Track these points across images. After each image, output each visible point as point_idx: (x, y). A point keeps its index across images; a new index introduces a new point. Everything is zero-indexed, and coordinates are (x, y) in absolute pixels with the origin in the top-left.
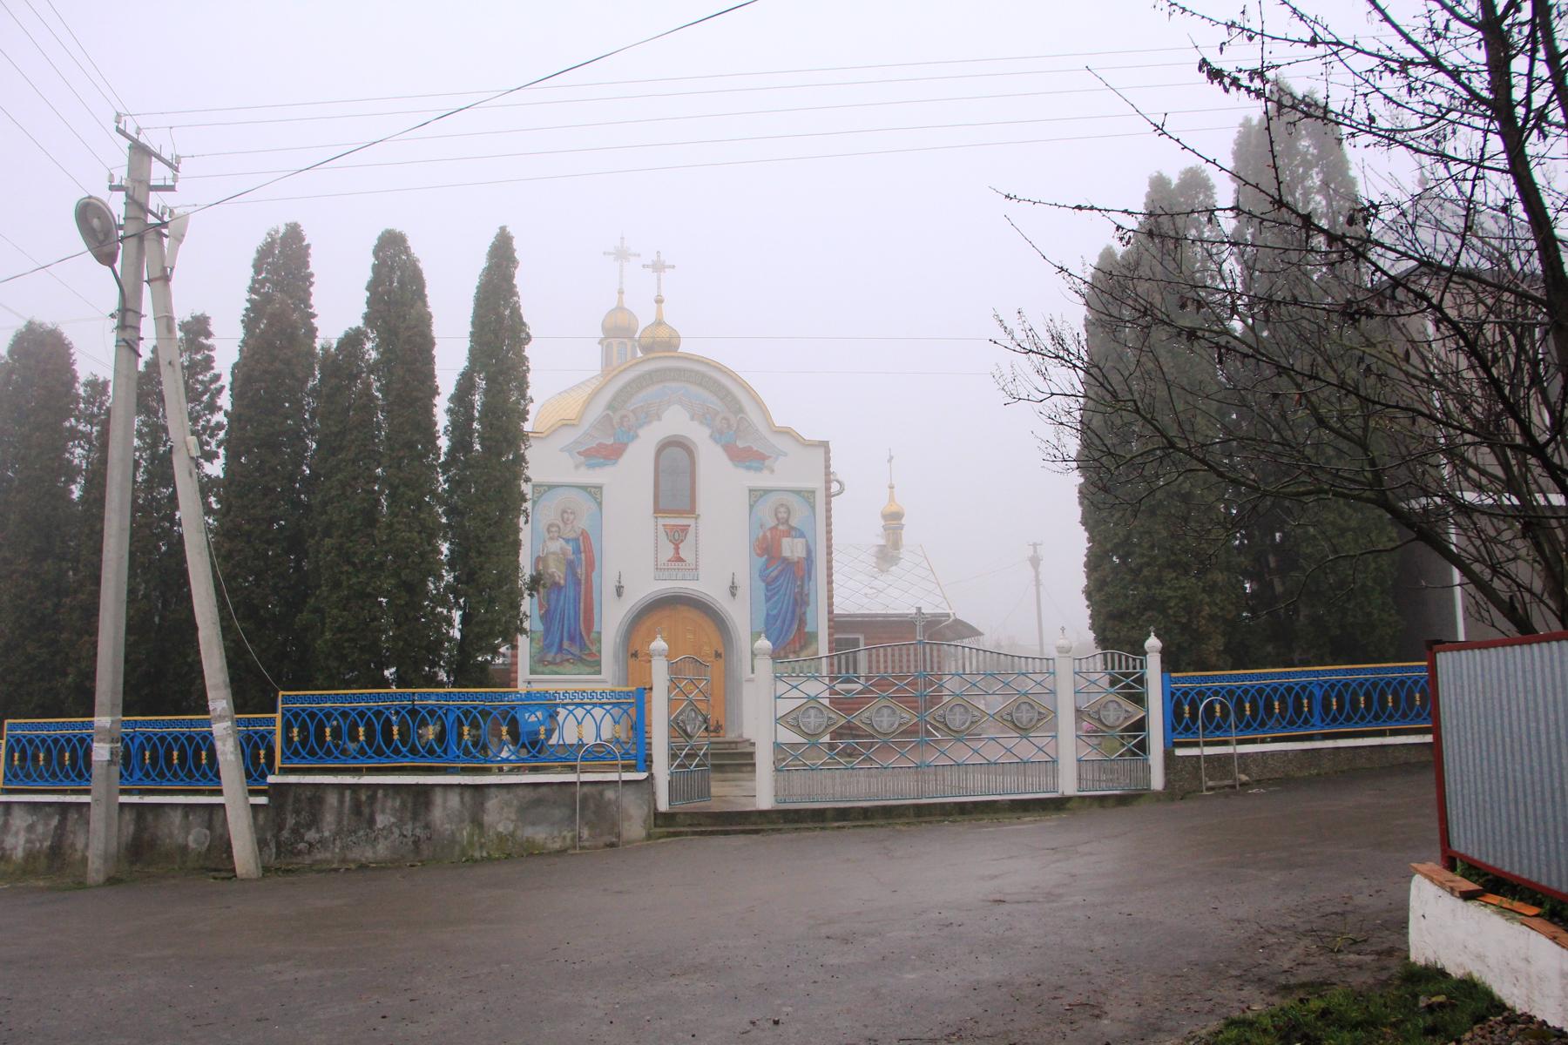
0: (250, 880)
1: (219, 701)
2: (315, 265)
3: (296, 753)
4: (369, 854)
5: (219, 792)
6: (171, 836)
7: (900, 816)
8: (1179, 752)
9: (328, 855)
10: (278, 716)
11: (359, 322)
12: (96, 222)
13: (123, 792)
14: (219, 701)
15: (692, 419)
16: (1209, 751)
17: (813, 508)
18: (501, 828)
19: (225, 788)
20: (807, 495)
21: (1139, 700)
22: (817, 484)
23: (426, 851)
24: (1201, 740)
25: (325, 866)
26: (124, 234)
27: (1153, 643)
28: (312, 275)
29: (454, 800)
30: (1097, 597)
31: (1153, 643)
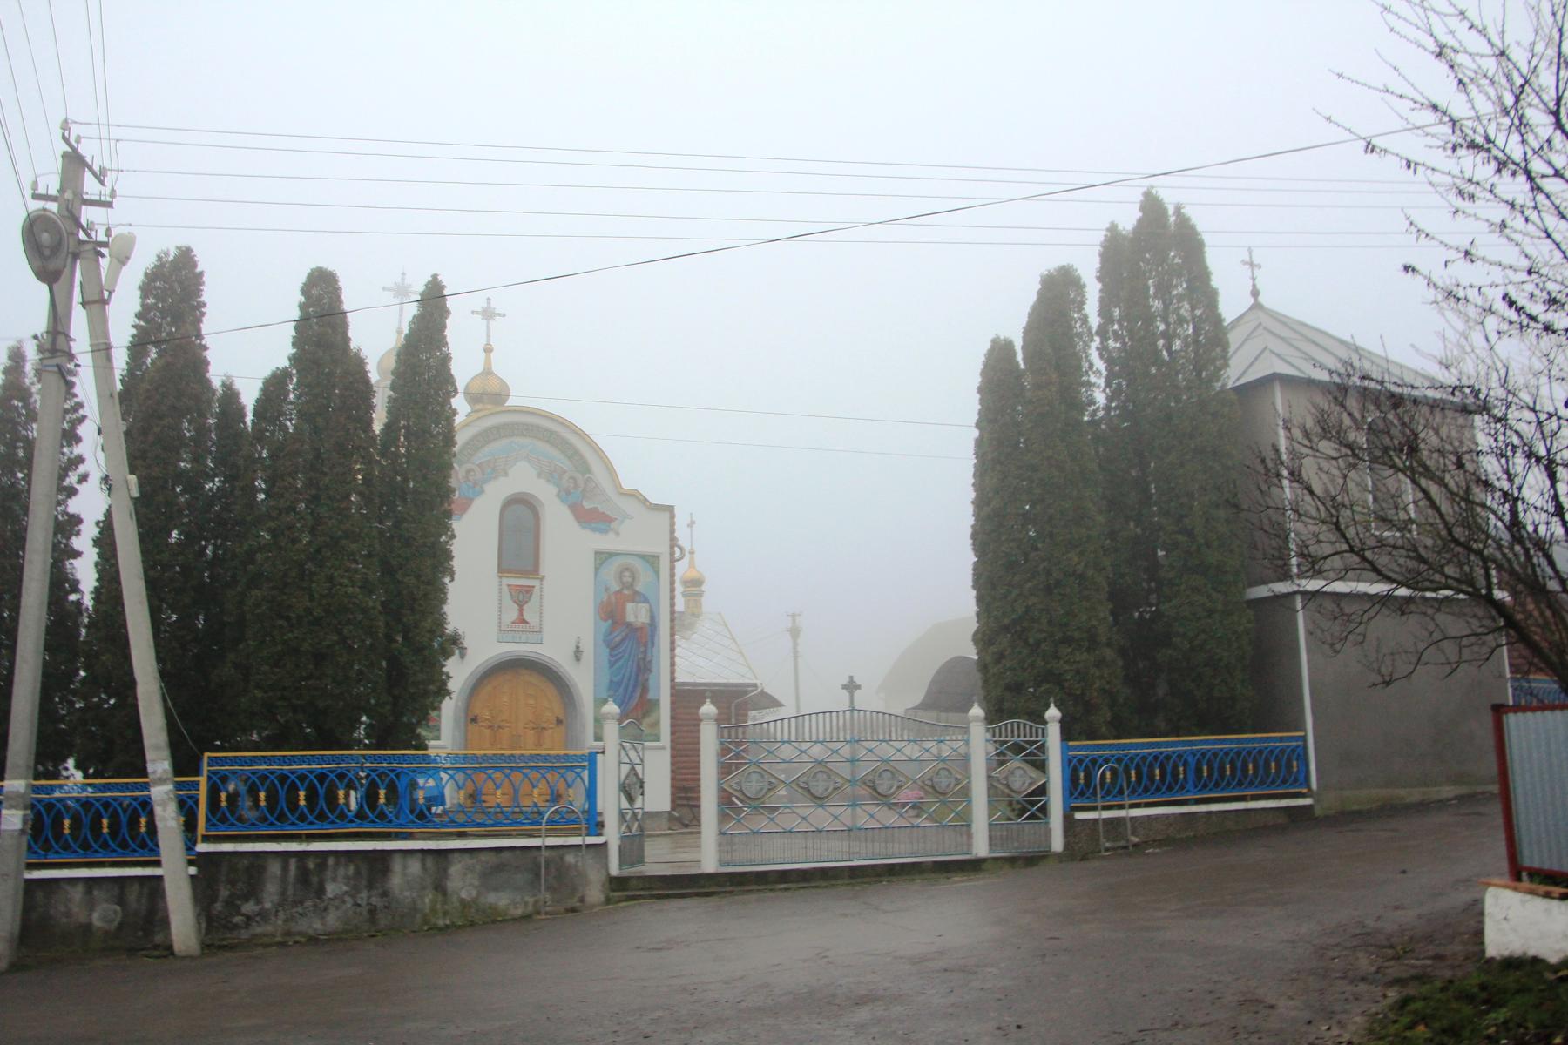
0: (192, 958)
1: (159, 763)
2: (208, 294)
3: (224, 820)
4: (317, 925)
5: (157, 864)
6: (68, 914)
7: (836, 877)
8: (1079, 816)
9: (269, 928)
10: (203, 780)
11: (284, 363)
12: (45, 238)
13: (31, 867)
14: (159, 763)
15: (539, 476)
16: (1106, 814)
17: (657, 573)
18: (464, 895)
19: (164, 858)
20: (652, 560)
21: (1041, 766)
22: (662, 549)
23: (384, 920)
24: (1100, 803)
25: (267, 940)
26: (56, 245)
27: (1053, 713)
28: (204, 305)
29: (415, 866)
30: (993, 670)
31: (1053, 713)
